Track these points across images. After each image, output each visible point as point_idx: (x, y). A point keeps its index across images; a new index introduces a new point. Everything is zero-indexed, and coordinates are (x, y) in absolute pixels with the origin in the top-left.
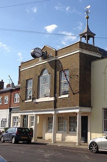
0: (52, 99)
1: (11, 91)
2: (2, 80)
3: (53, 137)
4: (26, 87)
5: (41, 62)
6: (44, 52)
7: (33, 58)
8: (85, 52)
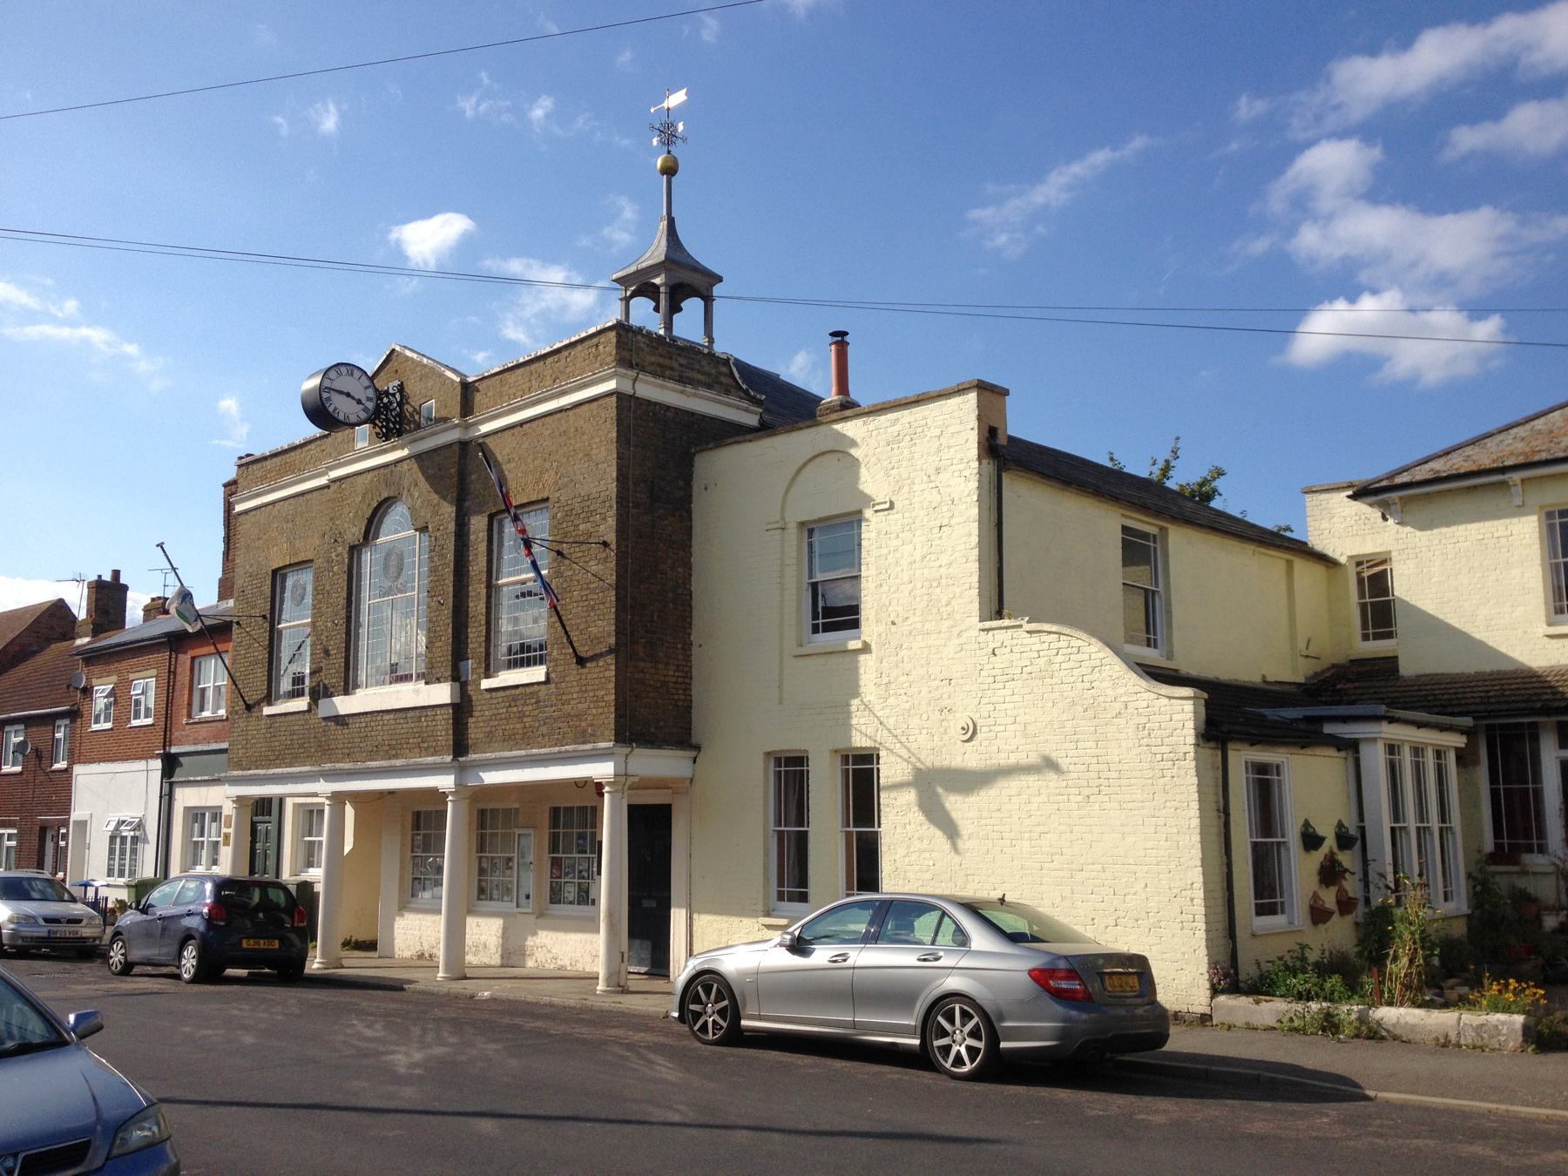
1: (176, 642)
2: (116, 574)
4: (272, 617)
5: (366, 454)
8: (653, 390)
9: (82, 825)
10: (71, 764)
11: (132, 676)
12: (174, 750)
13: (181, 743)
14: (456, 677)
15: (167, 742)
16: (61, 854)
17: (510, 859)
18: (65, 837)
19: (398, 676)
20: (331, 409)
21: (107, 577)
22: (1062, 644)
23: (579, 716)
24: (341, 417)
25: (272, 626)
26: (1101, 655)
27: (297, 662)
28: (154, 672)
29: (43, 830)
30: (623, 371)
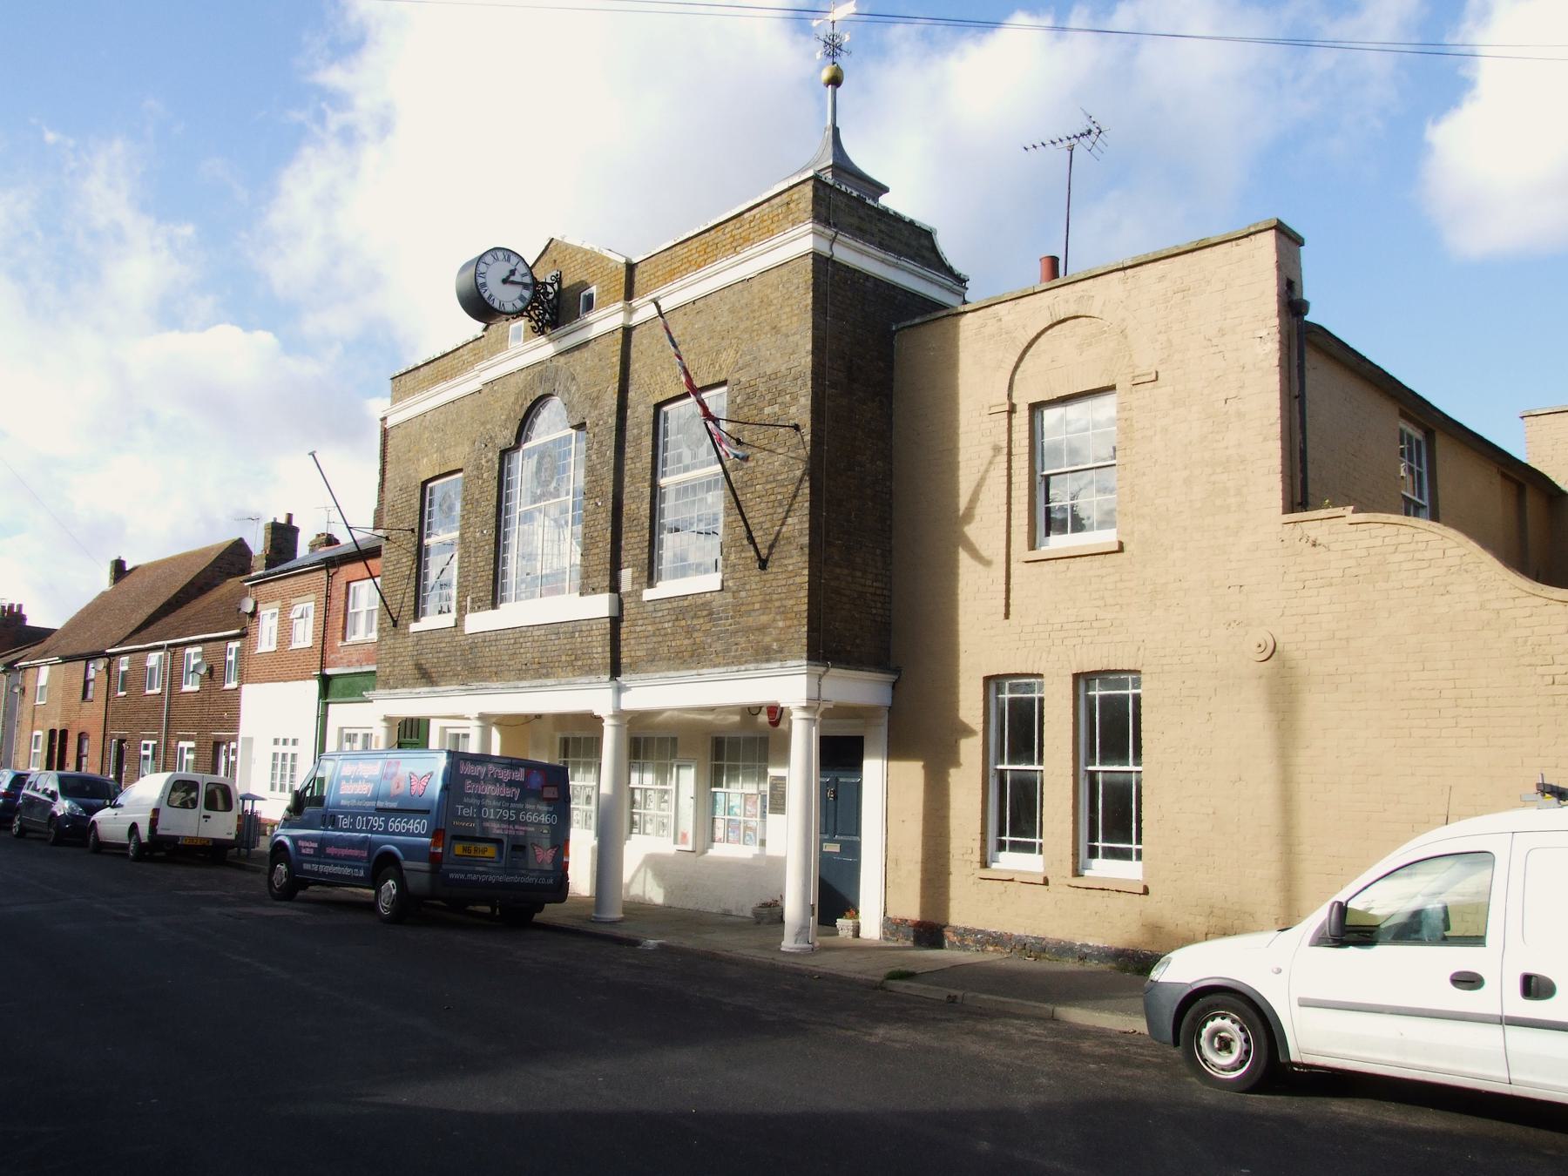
0: (599, 606)
1: (332, 564)
2: (290, 516)
3: (1497, 1119)
4: (420, 531)
5: (523, 350)
6: (544, 284)
7: (477, 327)
8: (854, 255)
9: (249, 741)
10: (241, 683)
11: (293, 601)
12: (329, 671)
13: (335, 665)
14: (615, 587)
15: (323, 666)
16: (231, 768)
17: (666, 792)
18: (235, 752)
19: (549, 585)
20: (486, 296)
21: (282, 520)
22: (1402, 539)
23: (762, 629)
24: (496, 305)
25: (421, 539)
26: (1462, 551)
27: (444, 566)
28: (313, 597)
29: (217, 745)
30: (821, 228)
